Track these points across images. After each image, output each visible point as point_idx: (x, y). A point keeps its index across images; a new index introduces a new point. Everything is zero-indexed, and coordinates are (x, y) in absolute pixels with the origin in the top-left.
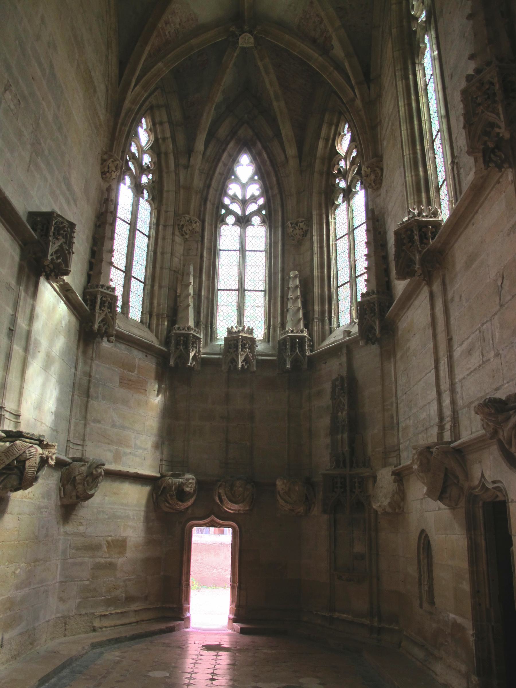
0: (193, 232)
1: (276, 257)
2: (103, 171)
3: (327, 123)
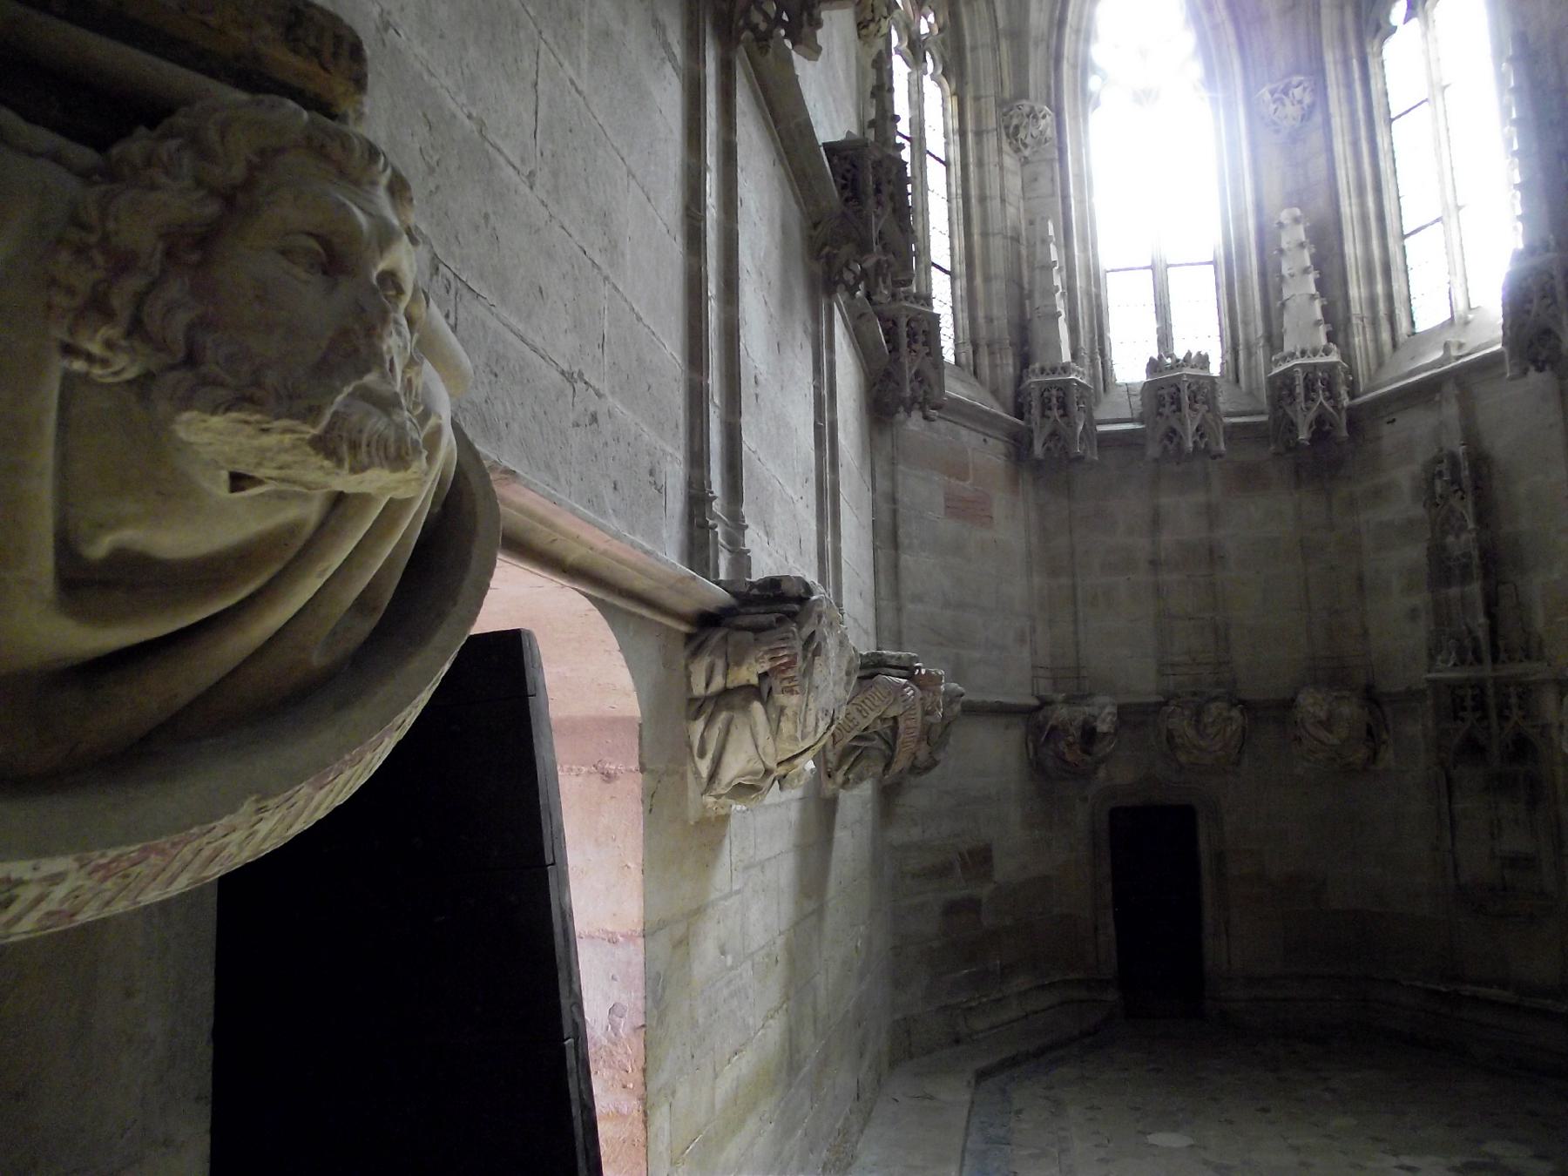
0: (1041, 140)
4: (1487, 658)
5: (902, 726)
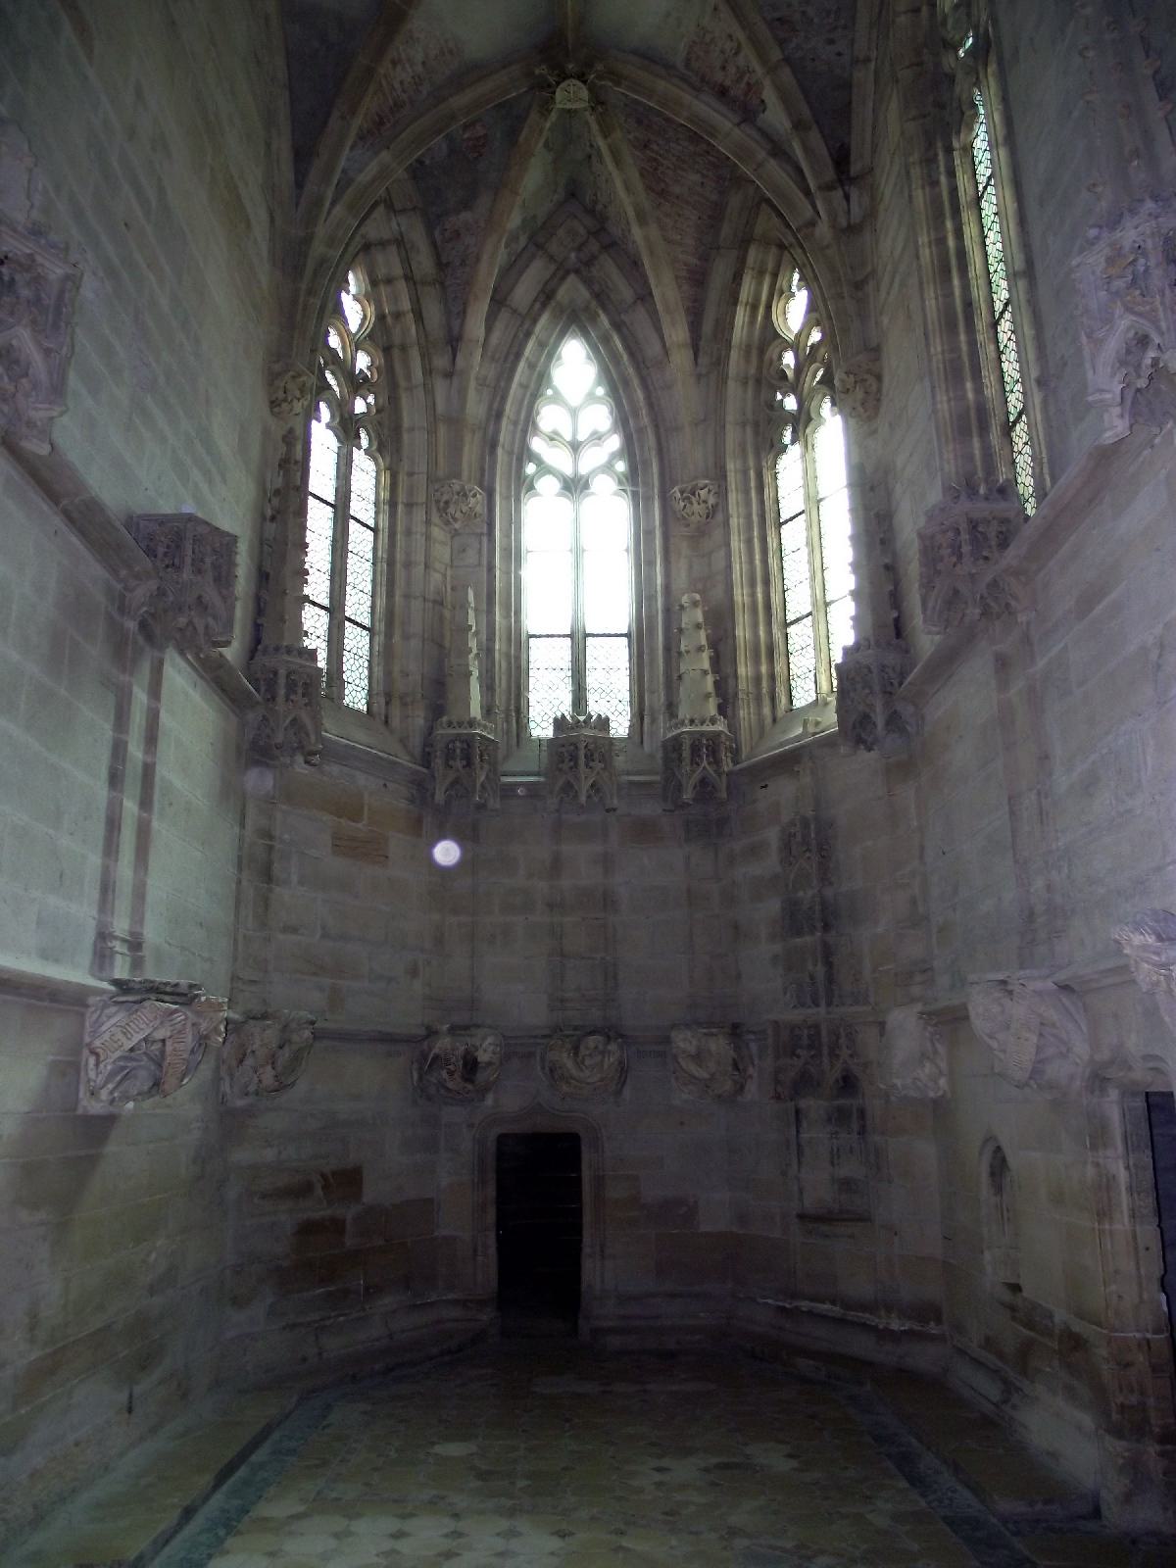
0: (470, 515)
1: (651, 563)
2: (273, 398)
3: (753, 269)
4: (823, 1003)
5: (169, 1048)
